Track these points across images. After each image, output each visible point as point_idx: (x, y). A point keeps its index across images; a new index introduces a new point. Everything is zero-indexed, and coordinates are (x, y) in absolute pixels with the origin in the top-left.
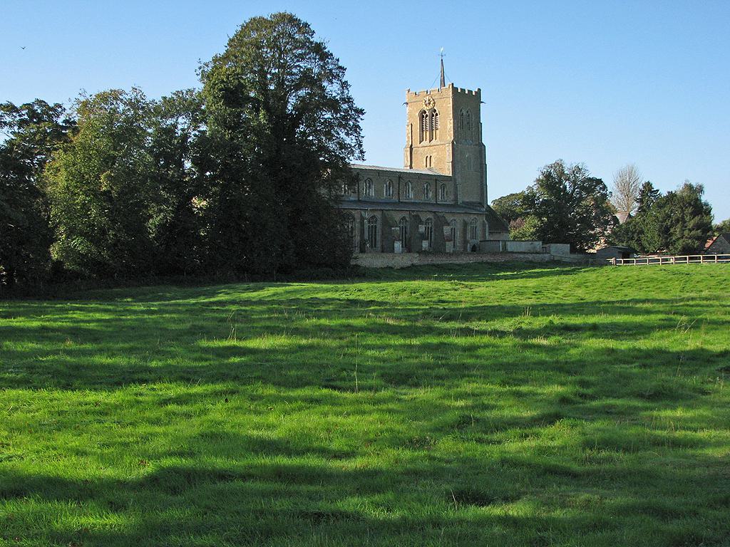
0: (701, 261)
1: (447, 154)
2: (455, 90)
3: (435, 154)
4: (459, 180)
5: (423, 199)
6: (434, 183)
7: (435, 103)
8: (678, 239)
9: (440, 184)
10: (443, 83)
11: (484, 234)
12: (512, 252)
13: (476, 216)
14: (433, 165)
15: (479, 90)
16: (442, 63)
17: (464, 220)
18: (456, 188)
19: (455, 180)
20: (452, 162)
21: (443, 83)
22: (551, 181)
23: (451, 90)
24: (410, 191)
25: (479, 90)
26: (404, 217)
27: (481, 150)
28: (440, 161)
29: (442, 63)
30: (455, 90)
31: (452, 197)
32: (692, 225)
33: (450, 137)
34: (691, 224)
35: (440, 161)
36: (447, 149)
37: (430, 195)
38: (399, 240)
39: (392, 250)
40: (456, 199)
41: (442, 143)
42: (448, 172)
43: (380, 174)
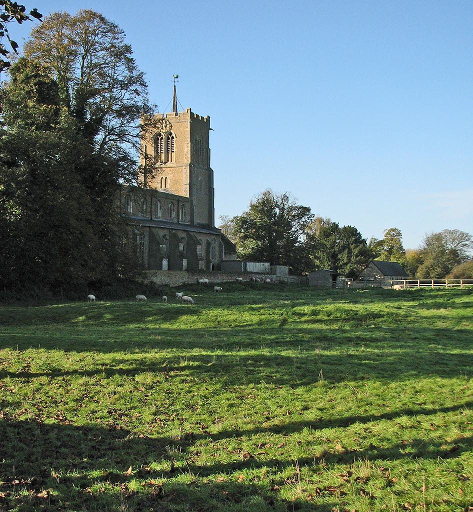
0: (432, 284)
1: (185, 176)
2: (192, 114)
3: (171, 175)
4: (195, 202)
5: (167, 219)
6: (177, 203)
7: (171, 126)
8: (346, 264)
9: (181, 204)
10: (8, 36)
11: (221, 256)
12: (251, 273)
13: (214, 237)
14: (168, 186)
15: (209, 117)
16: (175, 89)
17: (207, 241)
18: (192, 210)
19: (192, 201)
20: (190, 184)
21: (8, 36)
22: (265, 206)
23: (189, 114)
24: (159, 210)
25: (209, 117)
26: (165, 235)
27: (210, 173)
28: (176, 182)
29: (175, 89)
30: (192, 114)
31: (188, 218)
32: (356, 252)
33: (187, 160)
34: (356, 251)
35: (176, 182)
36: (184, 171)
37: (174, 214)
38: (166, 258)
39: (160, 267)
40: (192, 220)
41: (179, 165)
42: (184, 192)
43: (168, 196)
